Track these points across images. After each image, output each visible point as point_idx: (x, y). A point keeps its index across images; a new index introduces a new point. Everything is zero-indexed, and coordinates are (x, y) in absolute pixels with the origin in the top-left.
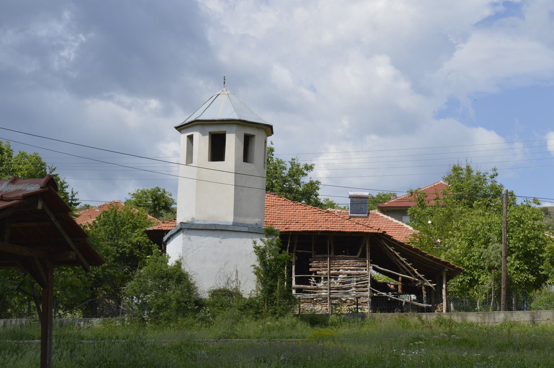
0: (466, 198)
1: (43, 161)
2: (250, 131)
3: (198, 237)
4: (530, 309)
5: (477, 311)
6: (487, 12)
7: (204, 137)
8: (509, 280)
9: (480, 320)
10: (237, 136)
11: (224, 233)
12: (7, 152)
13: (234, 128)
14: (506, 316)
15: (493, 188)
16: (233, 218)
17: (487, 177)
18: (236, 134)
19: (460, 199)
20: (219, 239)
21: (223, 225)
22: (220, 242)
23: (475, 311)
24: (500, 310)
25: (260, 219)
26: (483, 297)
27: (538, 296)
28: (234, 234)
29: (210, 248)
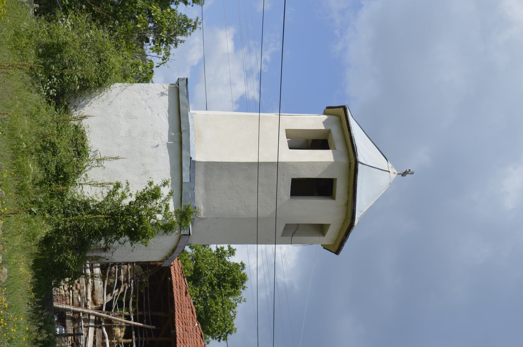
1: (235, 262)
2: (340, 189)
3: (167, 107)
7: (322, 124)
10: (331, 165)
11: (177, 147)
12: (234, 291)
13: (344, 160)
16: (202, 160)
18: (333, 163)
20: (167, 139)
21: (189, 143)
25: (204, 215)
28: (177, 162)
29: (152, 125)
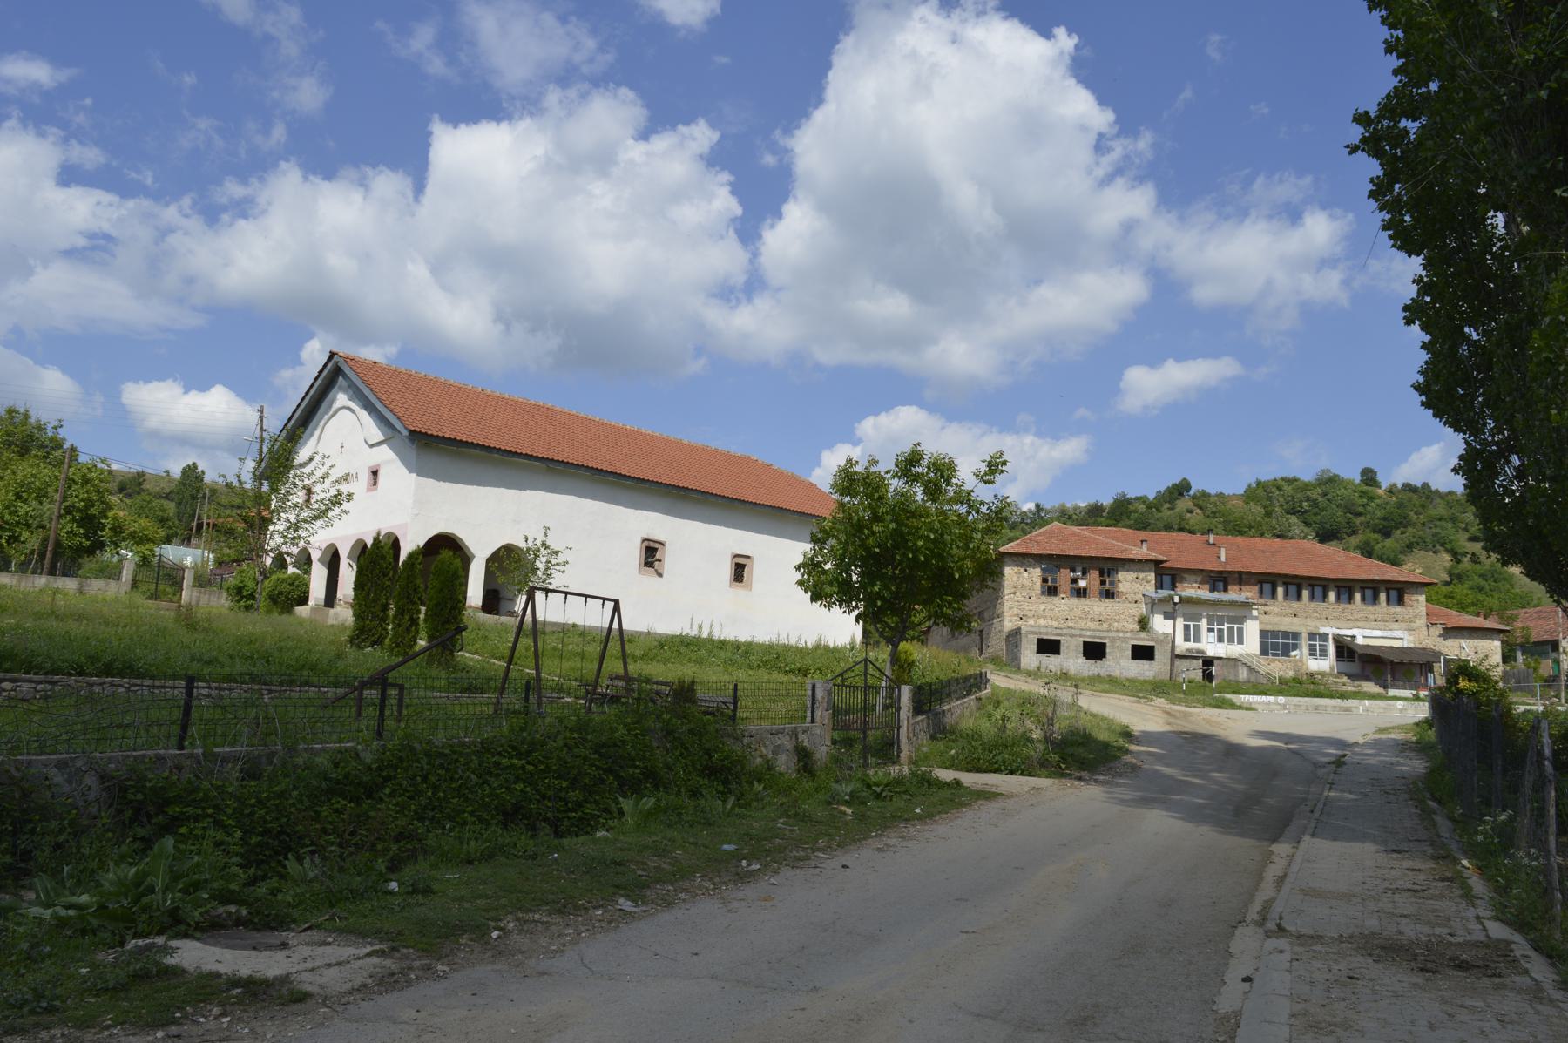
0: (16, 445)
4: (76, 576)
5: (11, 572)
6: (81, 242)
8: (58, 544)
9: (14, 582)
14: (49, 582)
15: (52, 440)
17: (49, 427)
19: (10, 446)
22: (651, 554)
23: (8, 572)
24: (41, 574)
26: (23, 558)
27: (88, 564)
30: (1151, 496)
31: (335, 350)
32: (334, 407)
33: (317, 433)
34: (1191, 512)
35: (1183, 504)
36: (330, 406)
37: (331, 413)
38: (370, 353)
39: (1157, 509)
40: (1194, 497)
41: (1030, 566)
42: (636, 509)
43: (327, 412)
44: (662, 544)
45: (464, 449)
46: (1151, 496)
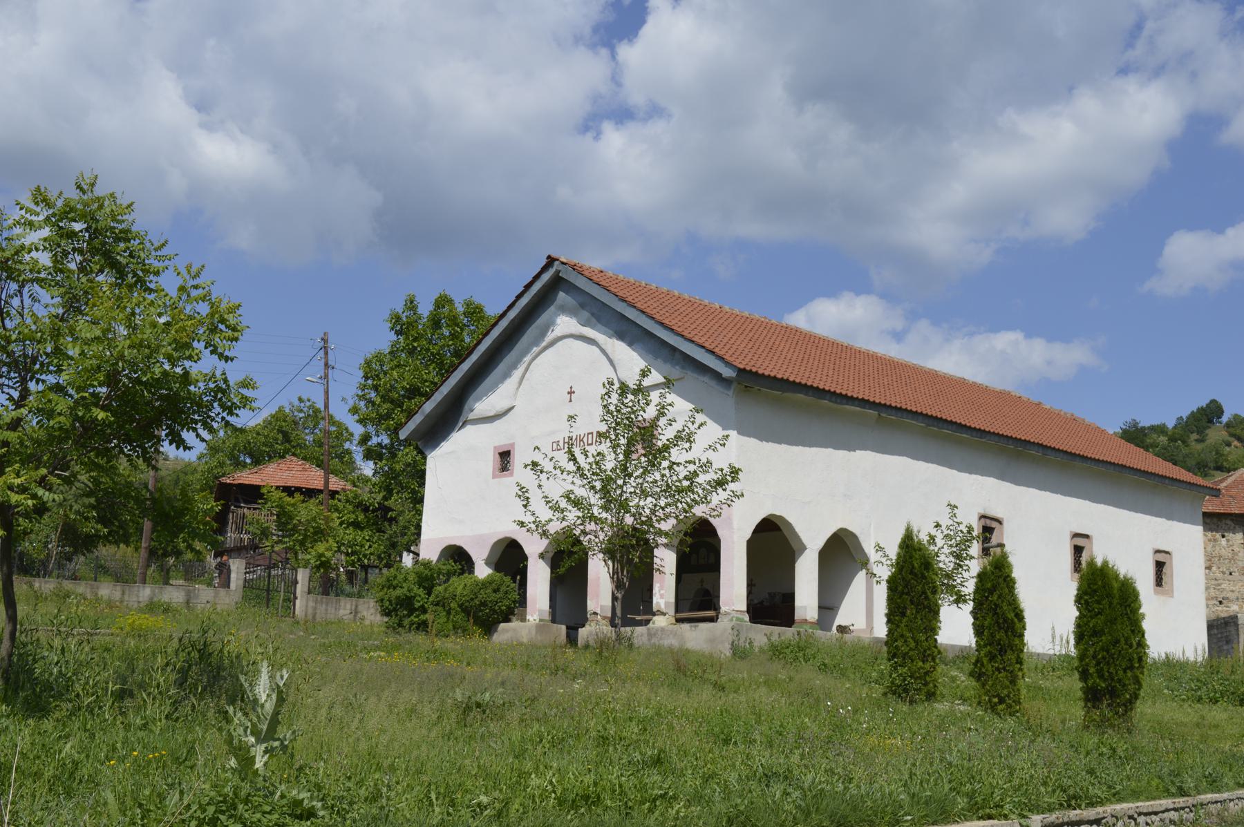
30: (1170, 424)
31: (554, 255)
32: (550, 336)
33: (517, 374)
34: (1229, 445)
35: (1216, 434)
36: (543, 334)
37: (544, 344)
38: (593, 260)
39: (1184, 442)
40: (1228, 425)
41: (1229, 530)
42: (970, 473)
43: (536, 342)
44: (999, 522)
45: (789, 395)
46: (1170, 424)
